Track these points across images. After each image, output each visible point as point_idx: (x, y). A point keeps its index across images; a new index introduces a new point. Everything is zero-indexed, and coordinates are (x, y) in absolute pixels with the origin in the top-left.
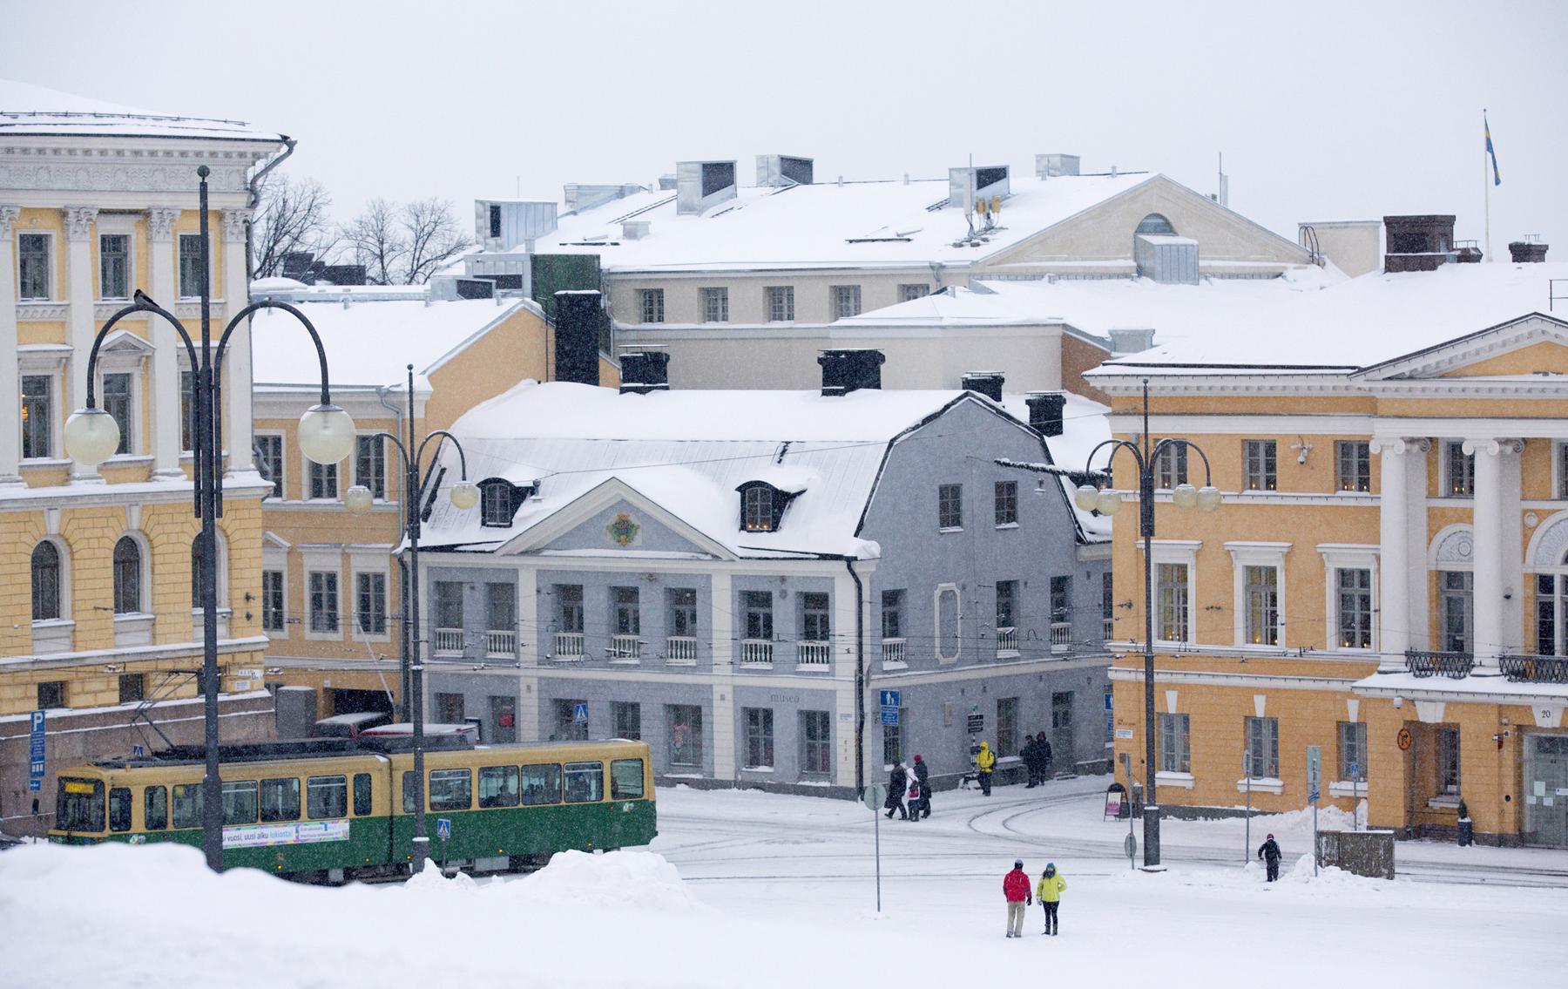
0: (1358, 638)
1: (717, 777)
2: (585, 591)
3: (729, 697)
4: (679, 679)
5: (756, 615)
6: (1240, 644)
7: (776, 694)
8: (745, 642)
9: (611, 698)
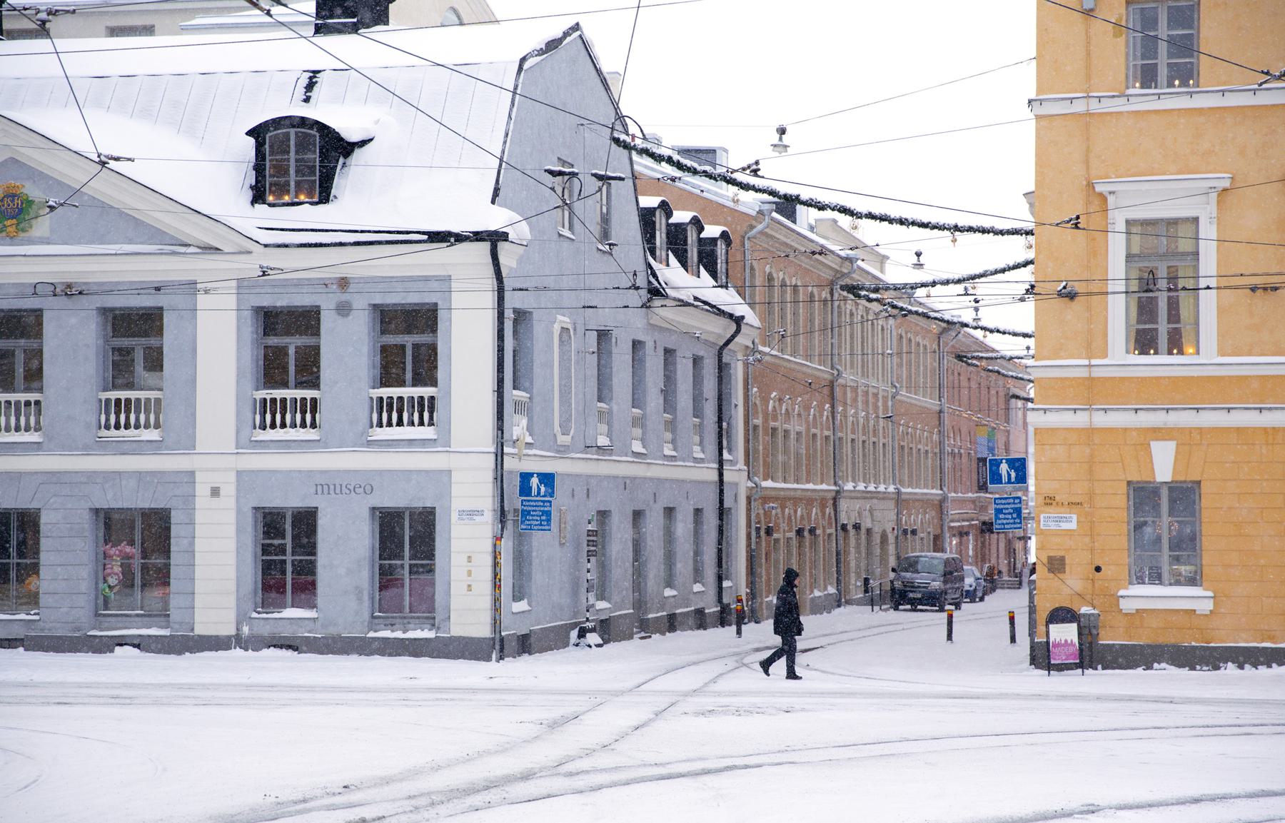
0: (1163, 341)
1: (200, 630)
2: (168, 319)
3: (229, 490)
4: (125, 467)
5: (285, 345)
6: (1119, 356)
7: (329, 483)
8: (104, 396)
9: (90, 505)
